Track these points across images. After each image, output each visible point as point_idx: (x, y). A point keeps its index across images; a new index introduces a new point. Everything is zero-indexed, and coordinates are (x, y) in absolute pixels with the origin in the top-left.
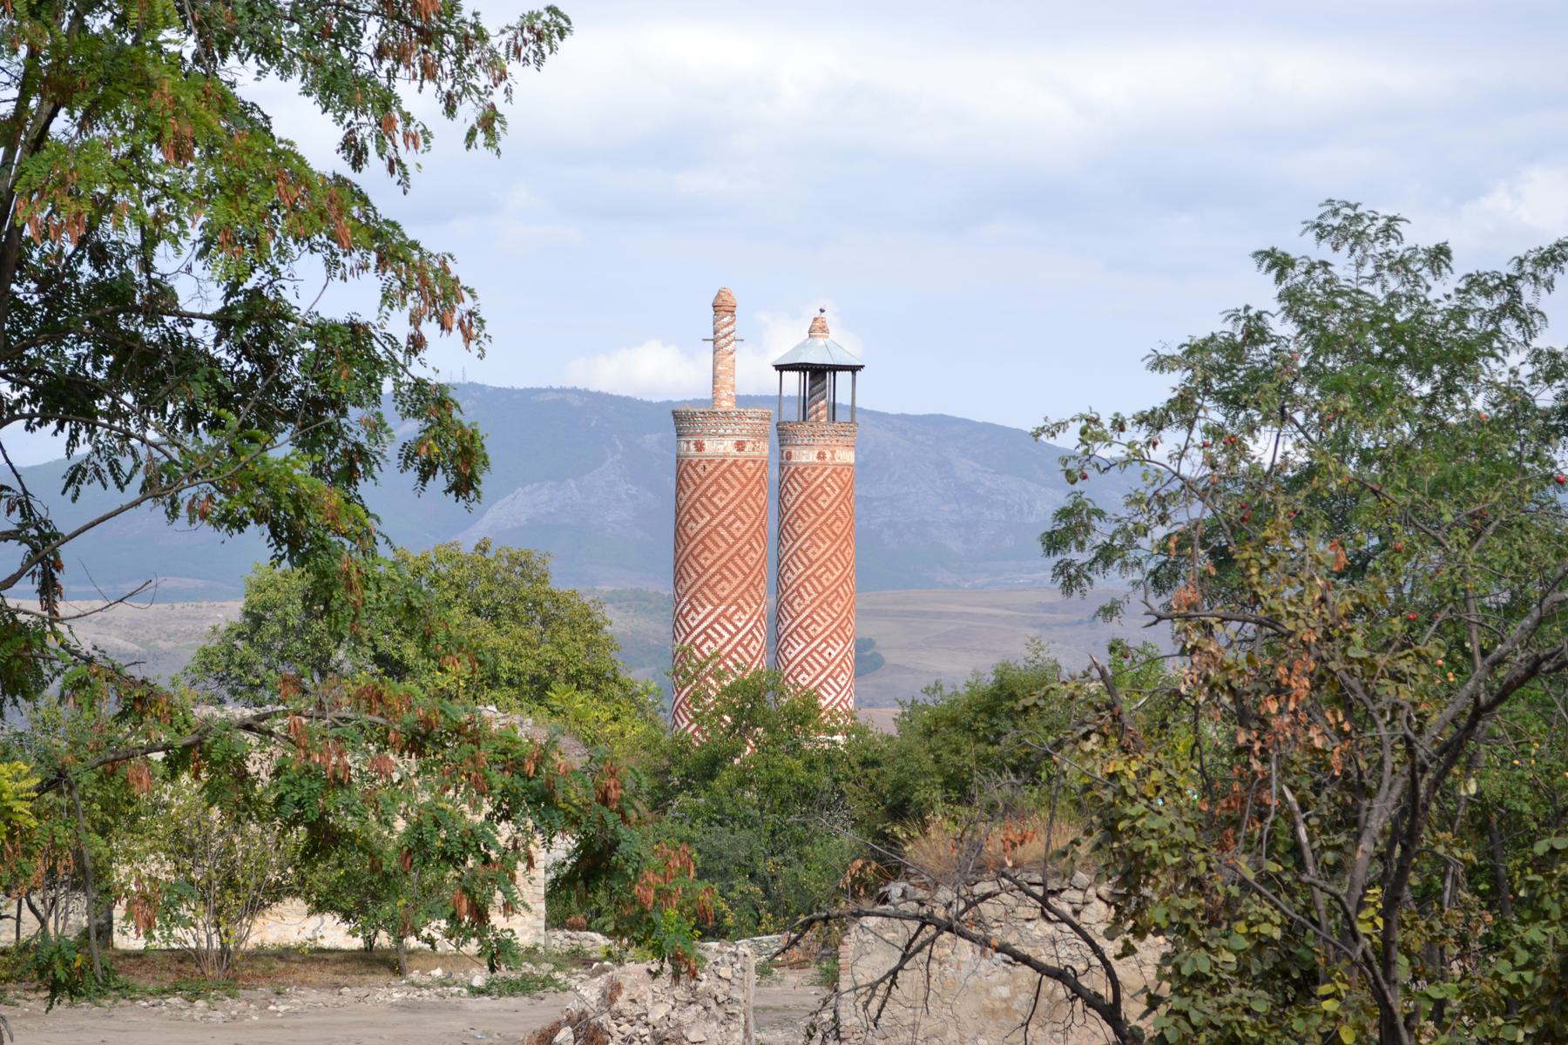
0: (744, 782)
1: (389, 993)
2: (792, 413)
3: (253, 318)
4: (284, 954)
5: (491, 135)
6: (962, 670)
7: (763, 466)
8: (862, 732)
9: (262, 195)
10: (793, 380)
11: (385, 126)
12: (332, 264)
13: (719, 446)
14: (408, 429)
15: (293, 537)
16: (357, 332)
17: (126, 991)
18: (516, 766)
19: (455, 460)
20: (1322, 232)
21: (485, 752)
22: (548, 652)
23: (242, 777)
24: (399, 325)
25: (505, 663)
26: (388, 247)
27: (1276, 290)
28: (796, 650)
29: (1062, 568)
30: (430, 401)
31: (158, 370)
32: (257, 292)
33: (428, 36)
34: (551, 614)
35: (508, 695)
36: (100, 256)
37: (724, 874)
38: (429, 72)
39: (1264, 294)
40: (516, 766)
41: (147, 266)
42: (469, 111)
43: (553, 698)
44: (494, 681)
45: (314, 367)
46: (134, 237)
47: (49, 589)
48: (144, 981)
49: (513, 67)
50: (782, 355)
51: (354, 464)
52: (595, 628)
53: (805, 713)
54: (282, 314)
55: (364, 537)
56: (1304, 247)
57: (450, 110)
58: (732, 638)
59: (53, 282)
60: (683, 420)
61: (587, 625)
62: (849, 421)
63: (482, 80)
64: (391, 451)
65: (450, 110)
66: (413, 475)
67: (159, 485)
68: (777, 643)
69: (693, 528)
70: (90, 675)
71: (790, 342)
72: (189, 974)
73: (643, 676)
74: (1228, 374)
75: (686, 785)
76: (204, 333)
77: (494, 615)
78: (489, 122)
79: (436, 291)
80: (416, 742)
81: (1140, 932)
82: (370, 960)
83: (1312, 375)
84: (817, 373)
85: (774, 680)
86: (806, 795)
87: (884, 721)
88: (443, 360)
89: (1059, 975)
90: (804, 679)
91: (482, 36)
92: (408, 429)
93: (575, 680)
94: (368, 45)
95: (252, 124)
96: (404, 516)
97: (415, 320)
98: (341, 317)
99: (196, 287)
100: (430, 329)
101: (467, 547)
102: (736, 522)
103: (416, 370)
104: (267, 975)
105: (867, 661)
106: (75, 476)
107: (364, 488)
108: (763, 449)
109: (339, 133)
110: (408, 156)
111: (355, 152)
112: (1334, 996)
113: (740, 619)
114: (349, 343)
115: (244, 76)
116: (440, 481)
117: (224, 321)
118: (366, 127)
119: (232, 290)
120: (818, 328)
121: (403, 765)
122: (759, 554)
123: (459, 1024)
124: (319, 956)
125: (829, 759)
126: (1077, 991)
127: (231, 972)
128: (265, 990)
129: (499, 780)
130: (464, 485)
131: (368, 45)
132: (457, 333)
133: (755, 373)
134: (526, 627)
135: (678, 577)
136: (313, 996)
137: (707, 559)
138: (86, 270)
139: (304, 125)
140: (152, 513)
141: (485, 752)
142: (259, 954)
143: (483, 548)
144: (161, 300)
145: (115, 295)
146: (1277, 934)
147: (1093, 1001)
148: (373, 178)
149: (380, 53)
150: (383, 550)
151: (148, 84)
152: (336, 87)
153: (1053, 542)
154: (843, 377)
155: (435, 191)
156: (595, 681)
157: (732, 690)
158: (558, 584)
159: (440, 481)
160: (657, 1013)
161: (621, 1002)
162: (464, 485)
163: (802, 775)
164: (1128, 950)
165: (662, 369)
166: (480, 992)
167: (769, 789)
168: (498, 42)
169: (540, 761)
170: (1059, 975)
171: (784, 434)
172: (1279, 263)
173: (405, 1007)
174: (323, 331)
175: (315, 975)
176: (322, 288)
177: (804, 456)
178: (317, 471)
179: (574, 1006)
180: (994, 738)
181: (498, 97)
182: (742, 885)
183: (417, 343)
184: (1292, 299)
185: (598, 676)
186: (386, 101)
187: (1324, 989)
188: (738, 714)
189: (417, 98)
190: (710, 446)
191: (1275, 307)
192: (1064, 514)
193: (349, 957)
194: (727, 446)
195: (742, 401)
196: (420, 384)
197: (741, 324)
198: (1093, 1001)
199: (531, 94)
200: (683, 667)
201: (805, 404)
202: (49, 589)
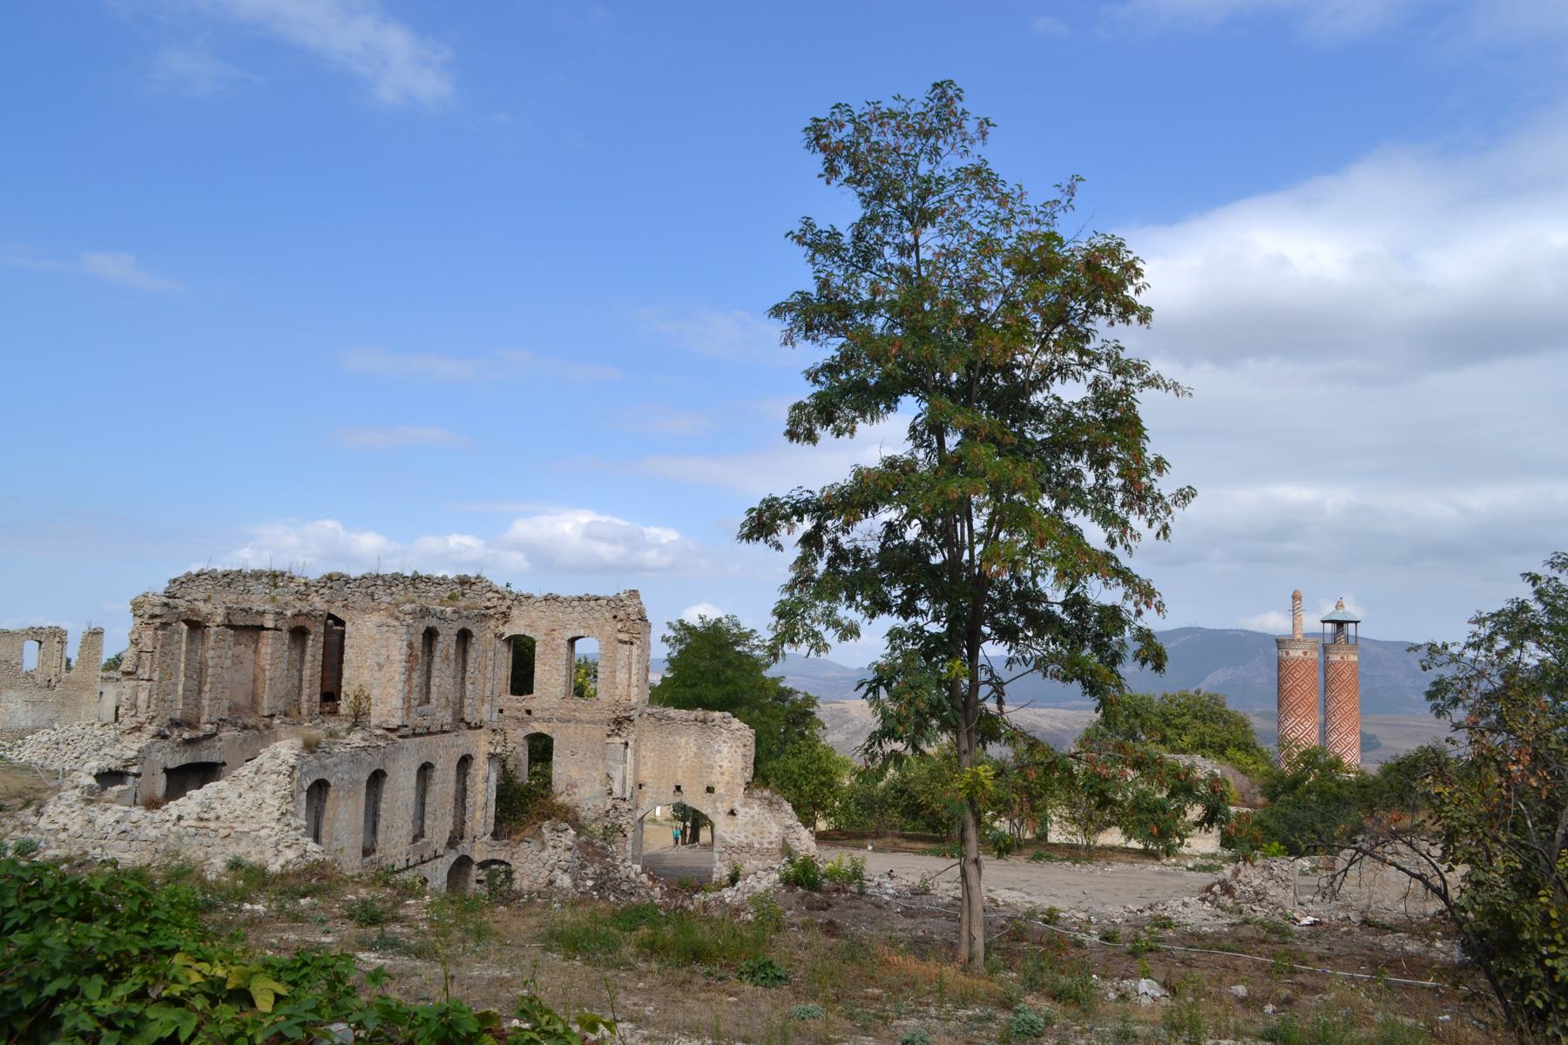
0: (1309, 791)
1: (1154, 867)
2: (1328, 640)
3: (1076, 604)
4: (1113, 849)
5: (1166, 536)
6: (1407, 747)
7: (1315, 661)
8: (1363, 773)
9: (1078, 561)
10: (1329, 627)
11: (1124, 533)
12: (1106, 583)
13: (1296, 653)
14: (1137, 646)
15: (1093, 687)
16: (1115, 610)
17: (1049, 858)
18: (1177, 776)
19: (1153, 653)
20: (1553, 565)
21: (1164, 770)
22: (1226, 735)
23: (1071, 774)
24: (1130, 606)
25: (1208, 739)
26: (1126, 576)
27: (1533, 590)
28: (1333, 738)
29: (1435, 707)
30: (1145, 636)
31: (1043, 622)
32: (1077, 594)
33: (1142, 498)
34: (1228, 719)
35: (1209, 752)
36: (1019, 582)
37: (1301, 829)
38: (1142, 511)
39: (1526, 592)
40: (1177, 776)
41: (1035, 584)
42: (1157, 526)
43: (1229, 752)
44: (1203, 745)
45: (1100, 622)
46: (1028, 573)
47: (1000, 702)
48: (1056, 855)
49: (1174, 508)
50: (1325, 616)
51: (1116, 658)
52: (1246, 726)
53: (1336, 764)
54: (1086, 602)
55: (1119, 686)
56: (1545, 572)
57: (1150, 525)
58: (1304, 731)
59: (1004, 589)
60: (1280, 642)
61: (1243, 724)
62: (1355, 644)
63: (1162, 514)
64: (1129, 653)
65: (1150, 525)
66: (1138, 663)
67: (1040, 664)
68: (1324, 734)
69: (1285, 686)
70: (1015, 736)
71: (1329, 610)
72: (1072, 853)
73: (1270, 747)
74: (1515, 623)
75: (1284, 791)
76: (1058, 609)
77: (1203, 719)
78: (1165, 528)
79: (1146, 593)
80: (1138, 764)
81: (1456, 862)
82: (1146, 854)
83: (1549, 627)
84: (1340, 624)
85: (1323, 751)
86: (1337, 798)
87: (1373, 770)
88: (1150, 620)
89: (1419, 877)
90: (1337, 750)
91: (1161, 497)
92: (1137, 646)
93: (1238, 747)
94: (1118, 502)
95: (1073, 532)
96: (1135, 678)
97: (1136, 604)
98: (1109, 603)
99: (1053, 592)
100: (1143, 607)
101: (1192, 692)
102: (1306, 686)
103: (1139, 623)
104: (1105, 856)
105: (1368, 743)
106: (1010, 661)
107: (1119, 668)
108: (1315, 655)
109: (1106, 536)
110: (1132, 543)
111: (1112, 542)
112: (1546, 896)
113: (1307, 724)
114: (1112, 615)
115: (1073, 516)
116: (1149, 665)
117: (1065, 604)
118: (1116, 533)
119: (1068, 593)
120: (1339, 605)
121: (1131, 774)
122: (1315, 697)
123: (1181, 882)
124: (1126, 851)
125: (1349, 783)
126: (1427, 885)
127: (1091, 854)
128: (1103, 862)
129: (1170, 781)
130: (1158, 667)
131: (1118, 502)
132: (1153, 609)
133: (1312, 622)
134: (1216, 727)
135: (1279, 706)
136: (1122, 866)
137: (1292, 699)
138: (1015, 587)
139: (1095, 535)
140: (1039, 674)
141: (1164, 770)
142: (1103, 848)
143: (1198, 692)
144: (1040, 597)
145: (1023, 596)
146: (1519, 866)
147: (1436, 891)
148: (1119, 551)
149: (1123, 505)
150: (1127, 691)
151: (1030, 520)
152: (1107, 519)
153: (1430, 695)
154: (1351, 626)
155: (1143, 552)
156: (1247, 747)
157: (1304, 753)
158: (1230, 707)
159: (1149, 665)
160: (1256, 882)
161: (1240, 877)
162: (1158, 667)
163: (1335, 790)
164: (1451, 869)
165: (1276, 622)
166: (1189, 869)
167: (1321, 794)
168: (1168, 500)
169: (1187, 775)
170: (1419, 877)
171: (1326, 648)
172: (1534, 579)
173: (1160, 873)
174: (1102, 609)
175: (1124, 858)
176: (1100, 592)
177: (1335, 658)
178: (1101, 661)
179: (1220, 876)
180: (1404, 780)
181: (1169, 520)
182: (1308, 834)
183: (1139, 613)
184: (1540, 595)
185: (1247, 745)
186: (1125, 523)
187: (1542, 892)
188: (1307, 764)
189: (1137, 522)
190: (1292, 653)
191: (1532, 597)
192: (1435, 684)
193: (1137, 851)
194: (1299, 653)
195: (1305, 635)
196: (1140, 628)
197: (1305, 603)
198: (1436, 891)
199: (1180, 517)
200: (1282, 743)
201: (1335, 636)
202: (1000, 702)
